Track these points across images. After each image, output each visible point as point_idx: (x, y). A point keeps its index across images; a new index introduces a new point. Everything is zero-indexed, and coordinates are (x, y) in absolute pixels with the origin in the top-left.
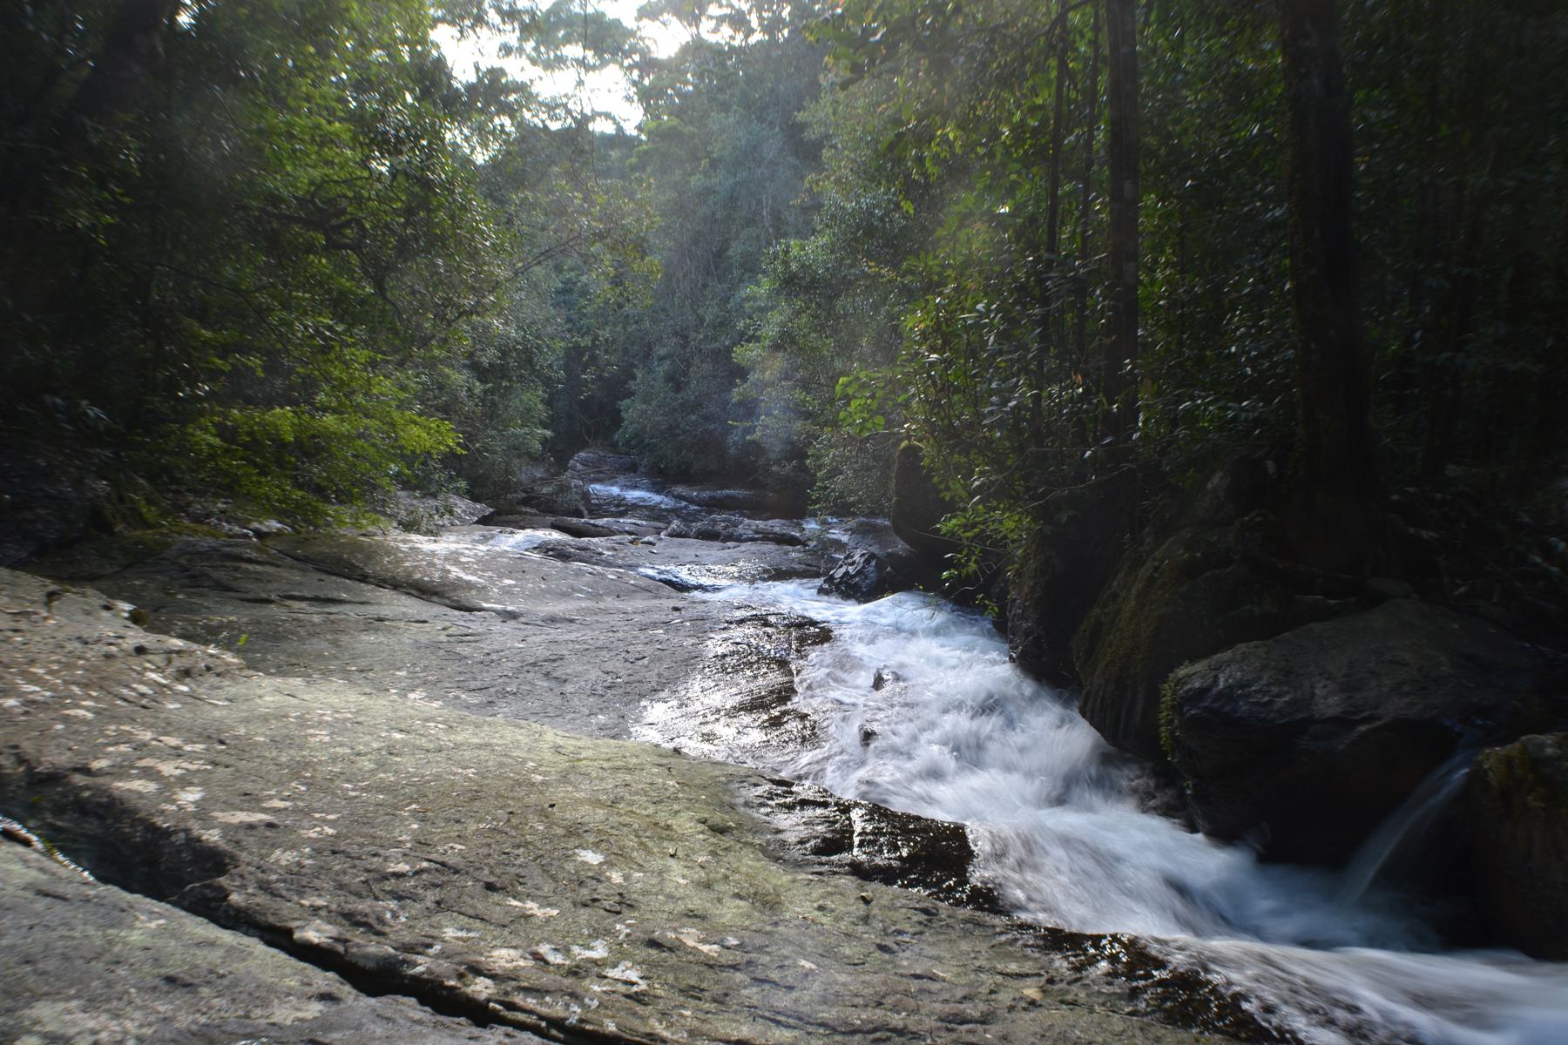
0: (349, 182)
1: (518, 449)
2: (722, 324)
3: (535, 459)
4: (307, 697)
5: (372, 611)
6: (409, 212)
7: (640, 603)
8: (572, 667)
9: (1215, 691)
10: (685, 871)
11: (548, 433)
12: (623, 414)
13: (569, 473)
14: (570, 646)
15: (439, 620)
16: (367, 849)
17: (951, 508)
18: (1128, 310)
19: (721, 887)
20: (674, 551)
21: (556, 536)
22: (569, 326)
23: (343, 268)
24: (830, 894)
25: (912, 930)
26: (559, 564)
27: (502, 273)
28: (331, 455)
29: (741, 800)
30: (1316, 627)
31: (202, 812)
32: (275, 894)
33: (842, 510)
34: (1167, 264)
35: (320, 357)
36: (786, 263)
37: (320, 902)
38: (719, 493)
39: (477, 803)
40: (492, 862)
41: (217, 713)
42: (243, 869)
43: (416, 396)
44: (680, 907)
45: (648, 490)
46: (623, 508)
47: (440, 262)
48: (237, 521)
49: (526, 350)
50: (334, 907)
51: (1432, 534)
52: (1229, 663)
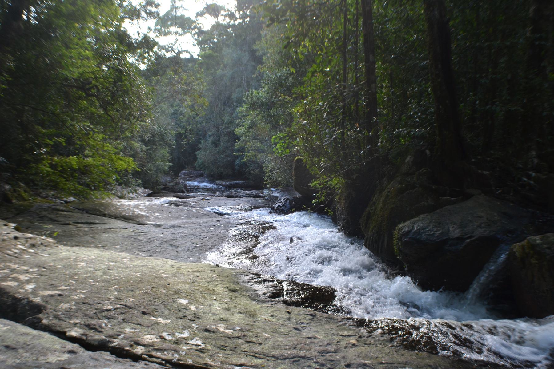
0: (93, 73)
1: (159, 170)
2: (231, 123)
3: (166, 173)
4: (79, 252)
5: (107, 226)
6: (115, 82)
7: (205, 220)
8: (180, 242)
9: (413, 231)
10: (220, 305)
11: (171, 164)
12: (198, 156)
13: (179, 178)
14: (180, 234)
15: (131, 228)
16: (96, 301)
17: (314, 177)
18: (373, 103)
19: (234, 310)
20: (217, 202)
21: (174, 199)
22: (177, 126)
23: (92, 104)
24: (275, 311)
25: (307, 322)
26: (175, 207)
27: (149, 103)
28: (91, 172)
29: (242, 281)
30: (448, 207)
31: (34, 292)
32: (60, 319)
33: (275, 185)
34: (386, 87)
35: (86, 137)
36: (252, 98)
37: (77, 321)
38: (233, 182)
39: (140, 284)
40: (145, 304)
41: (44, 259)
42: (48, 311)
43: (121, 151)
44: (218, 317)
45: (207, 183)
46: (197, 189)
47: (126, 99)
48: (58, 198)
49: (161, 135)
50: (82, 323)
51: (487, 172)
52: (418, 221)
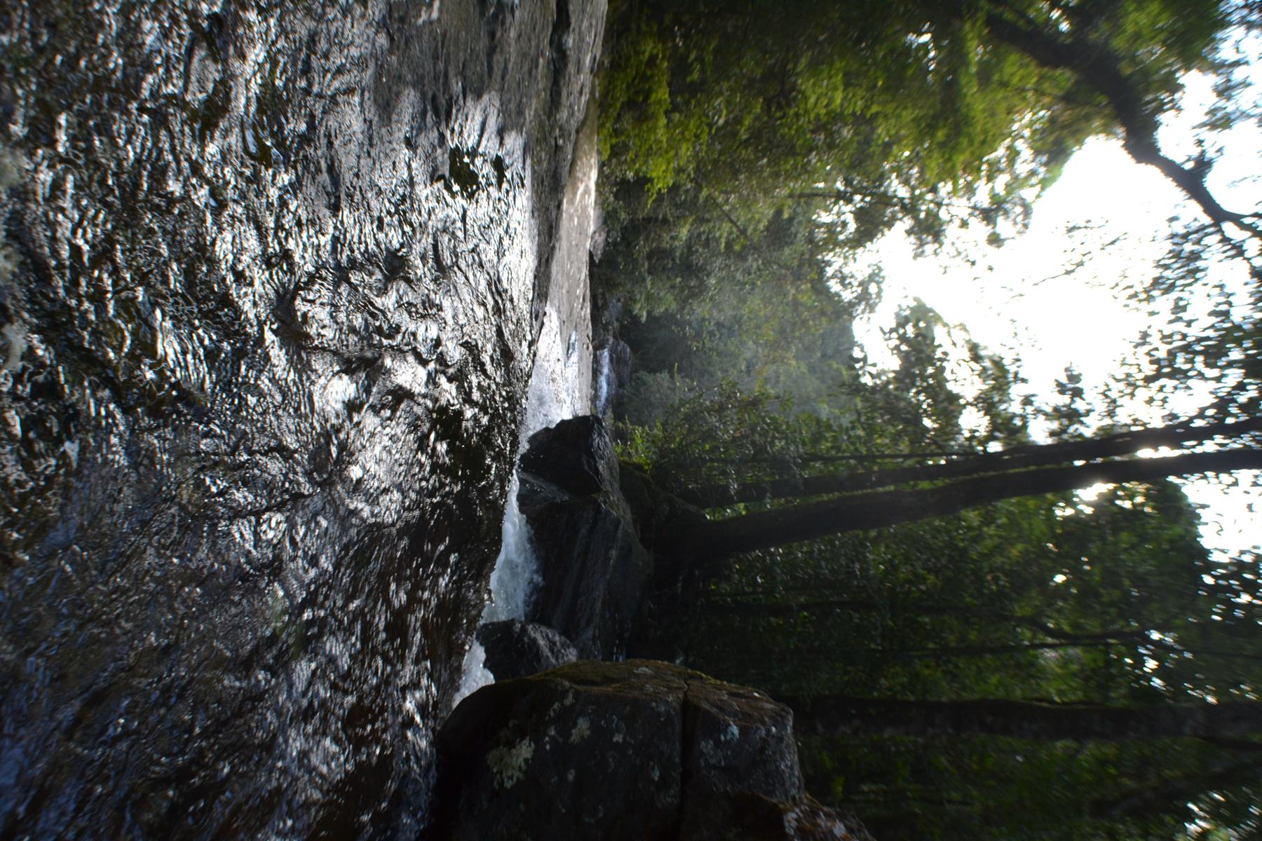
44: (526, 76)
